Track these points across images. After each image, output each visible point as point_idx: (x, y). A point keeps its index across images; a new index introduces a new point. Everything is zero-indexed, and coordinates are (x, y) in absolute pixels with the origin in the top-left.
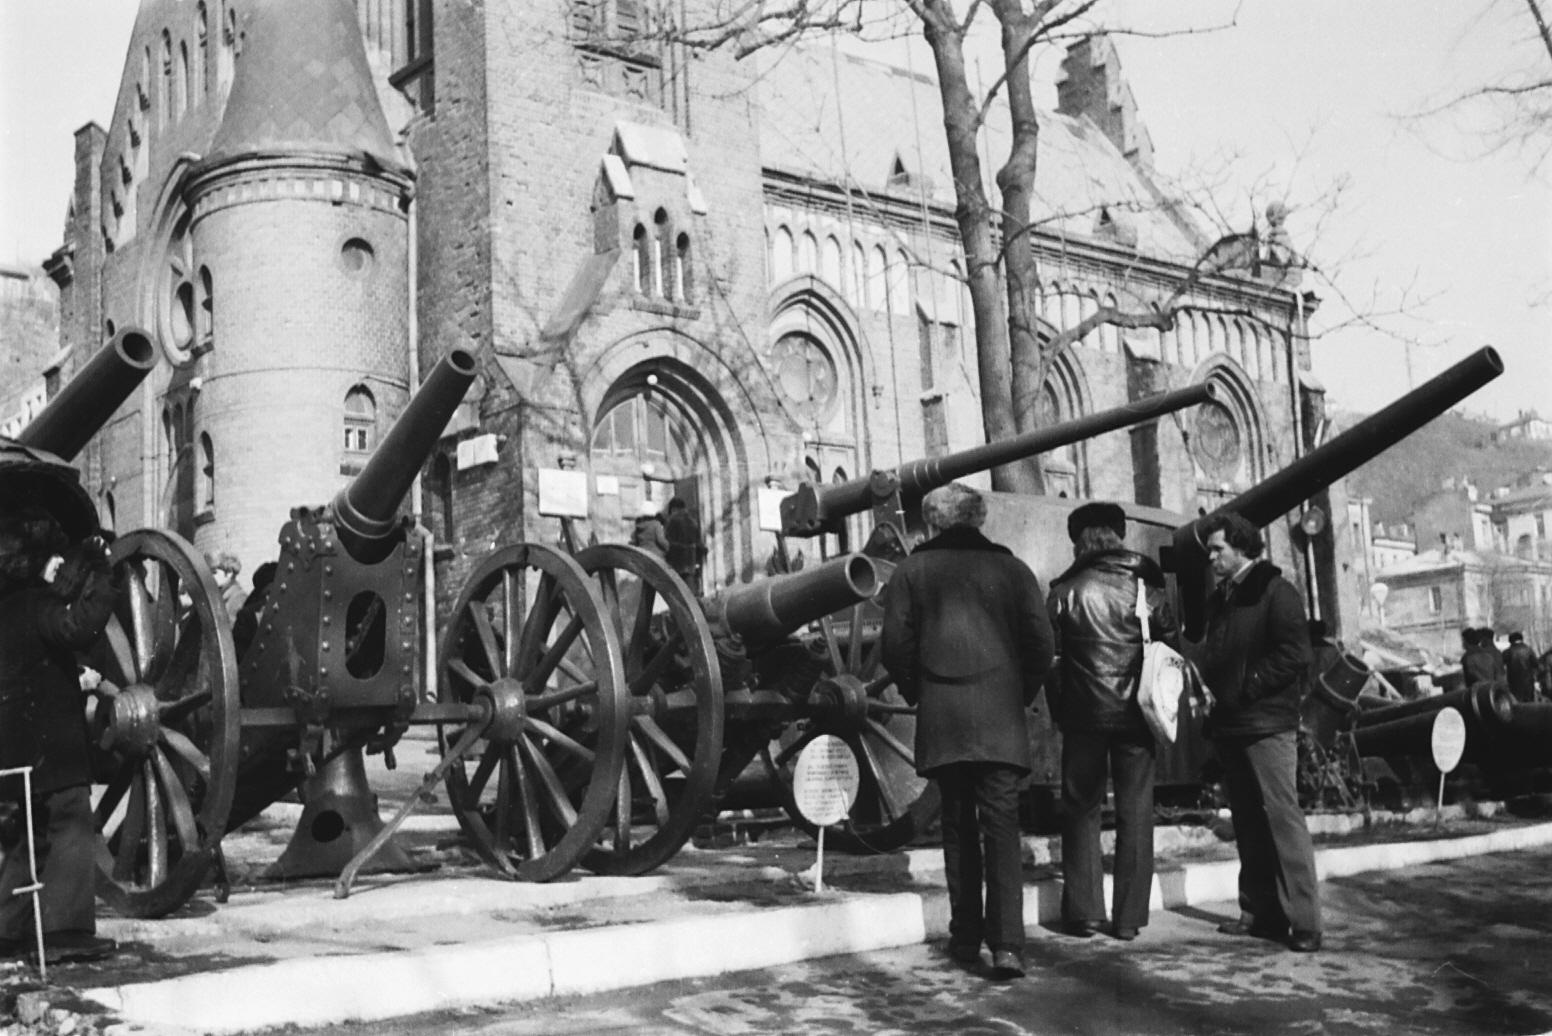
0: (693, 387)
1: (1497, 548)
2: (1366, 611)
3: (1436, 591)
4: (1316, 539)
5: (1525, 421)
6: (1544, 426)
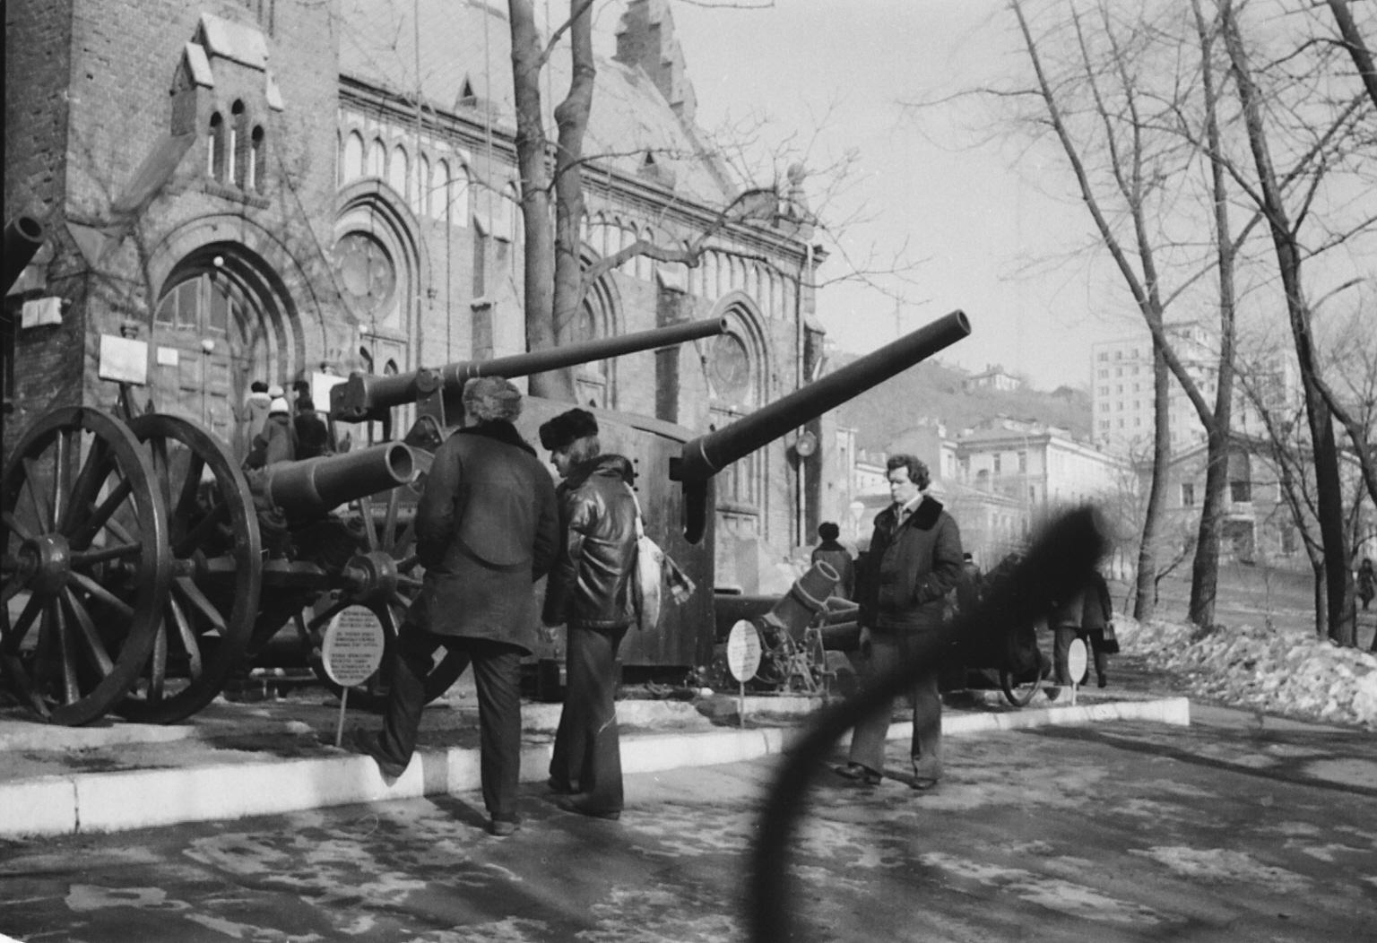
4: (806, 459)
5: (991, 374)
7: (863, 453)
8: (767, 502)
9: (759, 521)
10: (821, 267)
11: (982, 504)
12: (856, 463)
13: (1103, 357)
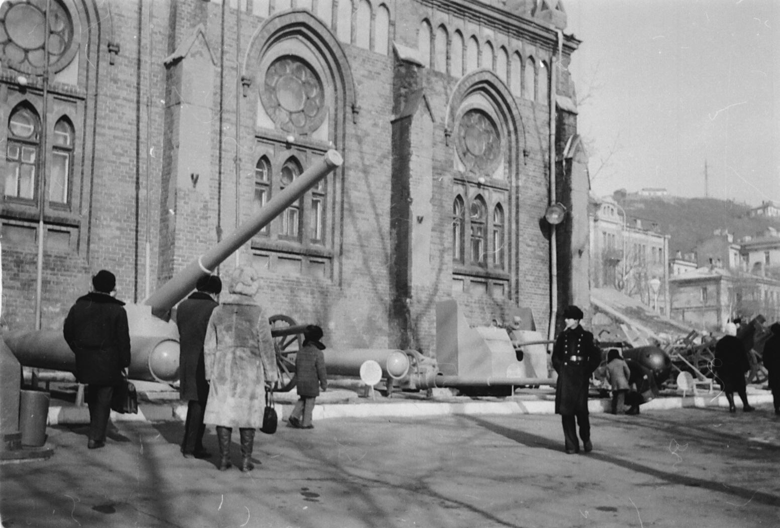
1: (741, 269)
3: (705, 290)
4: (558, 227)
5: (765, 206)
6: (775, 210)
8: (517, 269)
9: (510, 286)
10: (574, 55)
11: (757, 284)
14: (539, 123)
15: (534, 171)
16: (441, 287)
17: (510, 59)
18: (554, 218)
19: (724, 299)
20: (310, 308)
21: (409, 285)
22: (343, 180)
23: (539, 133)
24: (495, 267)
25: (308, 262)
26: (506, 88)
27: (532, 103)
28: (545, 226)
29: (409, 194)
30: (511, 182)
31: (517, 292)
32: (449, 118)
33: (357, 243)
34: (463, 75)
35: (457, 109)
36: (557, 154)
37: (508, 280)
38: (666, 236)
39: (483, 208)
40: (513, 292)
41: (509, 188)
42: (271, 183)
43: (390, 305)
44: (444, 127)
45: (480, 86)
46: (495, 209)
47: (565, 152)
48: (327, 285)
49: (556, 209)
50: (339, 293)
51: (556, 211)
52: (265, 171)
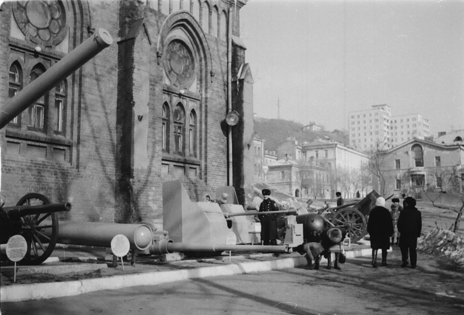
0: (409, 252)
2: (260, 177)
3: (283, 172)
4: (233, 127)
5: (311, 125)
7: (267, 151)
8: (206, 157)
9: (201, 169)
11: (312, 170)
12: (264, 154)
13: (353, 117)
14: (221, 53)
15: (217, 87)
16: (153, 169)
17: (202, 6)
18: (232, 121)
19: (294, 178)
20: (52, 185)
21: (132, 168)
22: (80, 85)
23: (220, 61)
24: (190, 155)
25: (52, 149)
26: (199, 26)
27: (216, 39)
28: (224, 126)
29: (132, 98)
30: (201, 95)
31: (206, 174)
32: (160, 43)
33: (91, 135)
34: (170, 13)
35: (165, 38)
36: (232, 77)
37: (199, 165)
38: (263, 140)
39: (182, 113)
40: (203, 174)
41: (200, 99)
42: (22, 84)
43: (116, 183)
44: (156, 50)
45: (181, 23)
46: (191, 114)
47: (239, 75)
48: (67, 167)
49: (233, 114)
50: (77, 174)
51: (233, 117)
52: (17, 74)
